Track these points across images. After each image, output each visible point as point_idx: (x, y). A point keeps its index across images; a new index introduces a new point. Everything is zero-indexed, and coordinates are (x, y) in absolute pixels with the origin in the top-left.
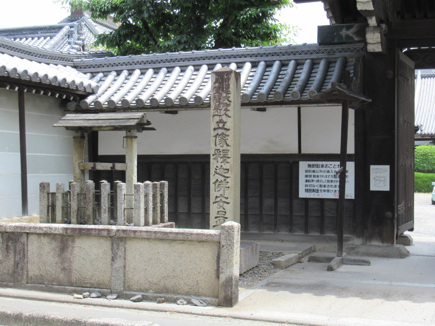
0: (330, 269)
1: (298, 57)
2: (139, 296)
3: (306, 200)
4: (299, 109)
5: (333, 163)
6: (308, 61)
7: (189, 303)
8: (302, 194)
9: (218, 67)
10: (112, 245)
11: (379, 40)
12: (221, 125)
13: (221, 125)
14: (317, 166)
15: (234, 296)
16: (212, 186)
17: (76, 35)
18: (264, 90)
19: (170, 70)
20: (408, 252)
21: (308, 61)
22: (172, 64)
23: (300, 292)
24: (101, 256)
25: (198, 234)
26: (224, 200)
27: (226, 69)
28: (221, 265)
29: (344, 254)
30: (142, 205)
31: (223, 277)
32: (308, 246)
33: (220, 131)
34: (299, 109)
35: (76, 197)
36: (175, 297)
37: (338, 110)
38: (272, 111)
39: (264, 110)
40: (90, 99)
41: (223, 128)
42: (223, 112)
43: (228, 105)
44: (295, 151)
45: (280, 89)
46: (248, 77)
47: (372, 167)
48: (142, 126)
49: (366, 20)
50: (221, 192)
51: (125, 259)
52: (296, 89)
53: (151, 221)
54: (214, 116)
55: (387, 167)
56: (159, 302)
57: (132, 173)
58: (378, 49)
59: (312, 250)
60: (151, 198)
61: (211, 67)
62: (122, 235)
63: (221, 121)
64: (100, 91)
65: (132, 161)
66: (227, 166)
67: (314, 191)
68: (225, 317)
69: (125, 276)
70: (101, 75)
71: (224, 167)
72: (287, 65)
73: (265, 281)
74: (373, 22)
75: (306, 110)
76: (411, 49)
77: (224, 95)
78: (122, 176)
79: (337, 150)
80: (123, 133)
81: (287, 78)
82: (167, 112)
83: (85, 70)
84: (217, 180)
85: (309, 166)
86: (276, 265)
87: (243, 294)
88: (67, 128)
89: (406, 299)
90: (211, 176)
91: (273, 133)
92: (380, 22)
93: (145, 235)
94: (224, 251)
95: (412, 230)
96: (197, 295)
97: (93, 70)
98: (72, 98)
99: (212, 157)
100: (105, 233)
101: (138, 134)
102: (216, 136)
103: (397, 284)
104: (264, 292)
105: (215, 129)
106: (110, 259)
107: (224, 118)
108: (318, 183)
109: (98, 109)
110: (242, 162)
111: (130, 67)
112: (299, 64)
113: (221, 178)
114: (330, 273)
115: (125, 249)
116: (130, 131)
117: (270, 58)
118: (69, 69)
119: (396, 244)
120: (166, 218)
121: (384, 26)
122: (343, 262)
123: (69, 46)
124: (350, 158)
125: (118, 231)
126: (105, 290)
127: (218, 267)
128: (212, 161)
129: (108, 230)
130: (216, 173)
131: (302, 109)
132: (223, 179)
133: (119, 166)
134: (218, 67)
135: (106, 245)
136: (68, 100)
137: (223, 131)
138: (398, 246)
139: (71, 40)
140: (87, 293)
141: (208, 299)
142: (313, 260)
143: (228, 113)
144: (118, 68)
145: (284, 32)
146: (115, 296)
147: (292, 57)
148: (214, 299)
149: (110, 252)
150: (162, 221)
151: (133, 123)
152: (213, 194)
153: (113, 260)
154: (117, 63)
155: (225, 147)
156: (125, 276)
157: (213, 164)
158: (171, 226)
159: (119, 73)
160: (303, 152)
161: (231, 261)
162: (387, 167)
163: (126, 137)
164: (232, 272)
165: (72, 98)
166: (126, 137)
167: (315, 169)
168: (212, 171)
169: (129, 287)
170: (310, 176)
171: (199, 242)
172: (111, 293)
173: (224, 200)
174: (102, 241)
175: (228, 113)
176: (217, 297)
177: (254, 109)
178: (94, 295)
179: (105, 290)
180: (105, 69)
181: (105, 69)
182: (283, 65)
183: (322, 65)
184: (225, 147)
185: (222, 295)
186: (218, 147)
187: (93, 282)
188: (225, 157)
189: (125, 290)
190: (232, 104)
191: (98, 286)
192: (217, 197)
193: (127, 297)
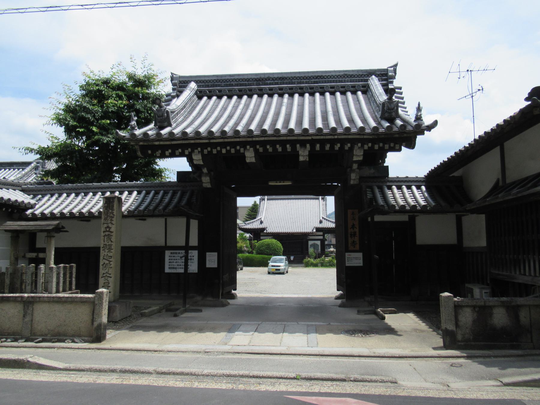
0: (175, 316)
1: (165, 189)
2: (40, 339)
3: (169, 274)
4: (166, 220)
5: (180, 251)
6: (171, 191)
7: (73, 341)
8: (167, 270)
9: (108, 194)
10: (24, 306)
11: (209, 181)
12: (108, 229)
13: (108, 229)
14: (176, 253)
15: (102, 335)
16: (101, 267)
17: (40, 169)
18: (142, 208)
19: (86, 194)
20: (229, 303)
21: (171, 191)
22: (88, 191)
23: (149, 331)
24: (16, 314)
25: (81, 298)
26: (108, 275)
27: (113, 195)
28: (95, 316)
29: (187, 306)
30: (55, 280)
31: (96, 324)
32: (169, 302)
33: (107, 233)
34: (166, 220)
35: (9, 276)
36: (65, 338)
37: (183, 220)
38: (150, 221)
39: (145, 220)
40: (29, 212)
41: (109, 231)
42: (109, 221)
43: (113, 217)
44: (163, 244)
45: (151, 208)
46: (130, 201)
47: (207, 253)
48: (58, 229)
49: (202, 170)
50: (107, 271)
51: (32, 315)
52: (161, 208)
53: (61, 289)
54: (104, 224)
55: (216, 254)
56: (53, 342)
57: (50, 259)
58: (209, 186)
59: (170, 304)
60: (62, 275)
61: (103, 193)
62: (31, 300)
63: (108, 227)
64: (37, 206)
65: (50, 252)
66: (111, 254)
67: (174, 268)
68: (93, 349)
69: (32, 326)
70: (40, 196)
71: (109, 255)
72: (168, 193)
73: (131, 325)
74: (205, 170)
75: (170, 220)
76: (289, 183)
77: (110, 211)
78: (43, 261)
79: (183, 244)
80: (45, 234)
81: (157, 201)
82: (82, 221)
83: (29, 193)
84: (104, 263)
85: (171, 253)
86: (143, 315)
87: (110, 334)
88: (6, 231)
89: (211, 331)
90: (101, 261)
91: (150, 234)
92: (209, 171)
93: (46, 299)
94: (97, 307)
95: (235, 289)
96: (79, 336)
97: (35, 193)
98: (16, 211)
99: (101, 249)
100: (20, 299)
101: (56, 235)
102: (104, 236)
103: (211, 322)
104: (127, 331)
105: (104, 232)
106: (22, 315)
107: (110, 225)
108: (173, 264)
109: (34, 218)
110: (122, 251)
111: (60, 192)
112: (166, 193)
113: (107, 262)
114: (175, 318)
115: (33, 309)
116: (50, 233)
117: (149, 189)
118: (17, 192)
119: (222, 298)
120: (74, 287)
121: (212, 173)
122: (186, 311)
123: (35, 176)
124: (193, 248)
125: (28, 297)
126: (18, 337)
127: (93, 318)
128: (101, 251)
129: (22, 297)
130: (104, 259)
131: (168, 219)
132: (108, 262)
133: (41, 255)
134: (108, 194)
135: (20, 307)
136: (12, 212)
137: (109, 233)
138: (222, 300)
139: (37, 172)
140: (4, 339)
141: (86, 338)
142: (168, 310)
143: (112, 222)
144: (52, 192)
145: (167, 173)
146: (23, 341)
147: (162, 188)
148: (89, 339)
149: (23, 312)
150: (70, 289)
151: (51, 228)
152: (102, 271)
153: (24, 316)
154: (51, 189)
155: (110, 243)
156: (32, 326)
157: (102, 253)
158: (77, 293)
159: (52, 195)
160: (168, 245)
161: (101, 313)
162: (216, 254)
163: (47, 236)
164: (101, 320)
165: (16, 211)
166: (47, 236)
167: (175, 255)
168: (101, 258)
169: (34, 333)
170: (172, 259)
171: (82, 302)
172: (22, 338)
173: (108, 275)
174: (17, 304)
175: (112, 222)
176: (92, 337)
177: (137, 219)
178: (9, 340)
179: (18, 337)
180: (43, 193)
181: (43, 193)
182: (157, 193)
183: (178, 195)
184: (110, 243)
185: (95, 335)
186: (106, 243)
187: (9, 331)
188: (110, 249)
189: (31, 335)
190: (115, 217)
191: (14, 334)
192: (104, 274)
193: (32, 340)
